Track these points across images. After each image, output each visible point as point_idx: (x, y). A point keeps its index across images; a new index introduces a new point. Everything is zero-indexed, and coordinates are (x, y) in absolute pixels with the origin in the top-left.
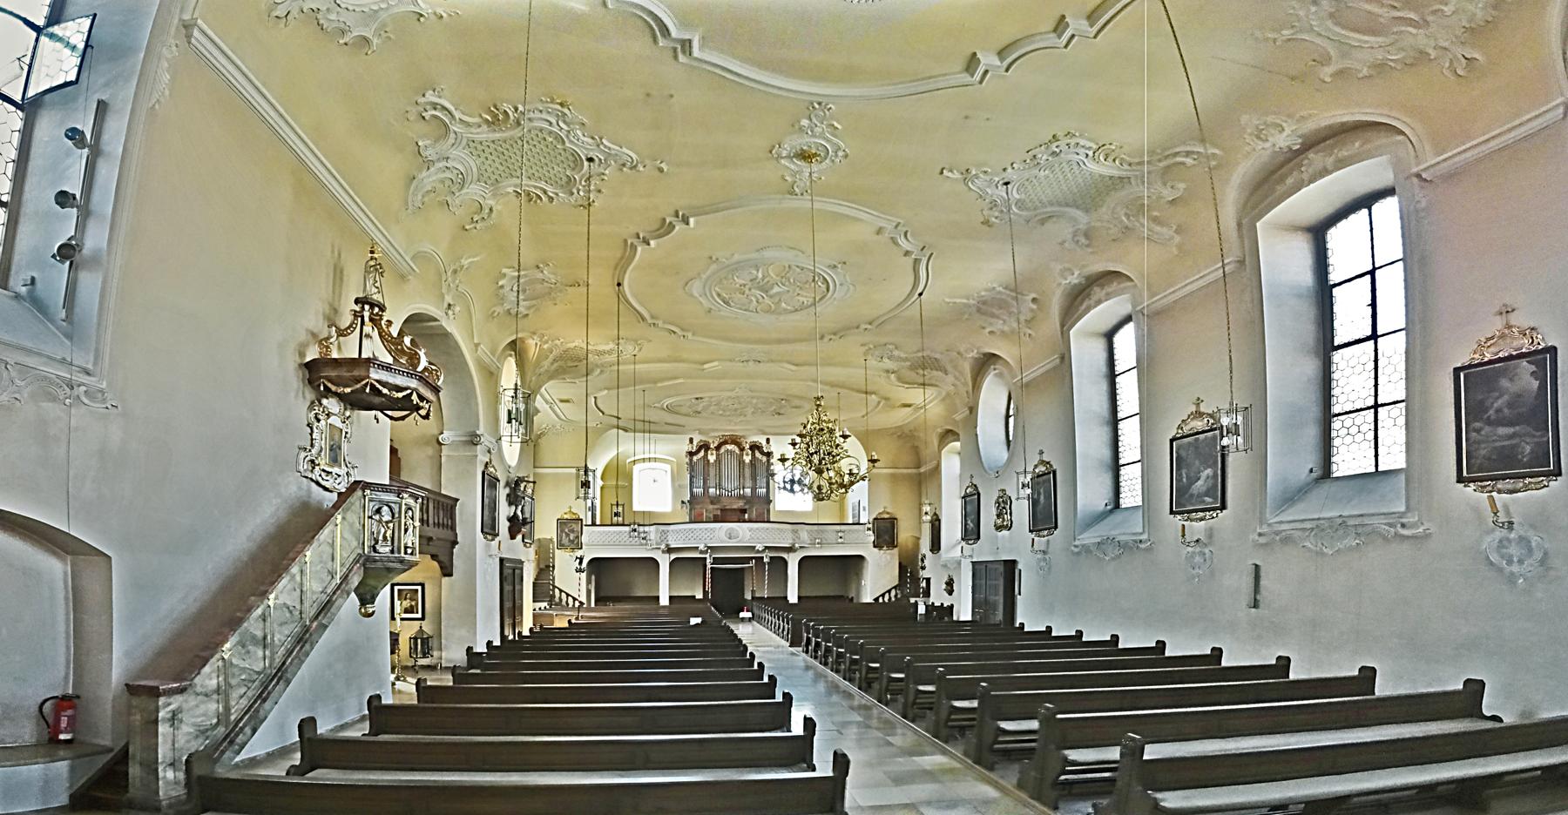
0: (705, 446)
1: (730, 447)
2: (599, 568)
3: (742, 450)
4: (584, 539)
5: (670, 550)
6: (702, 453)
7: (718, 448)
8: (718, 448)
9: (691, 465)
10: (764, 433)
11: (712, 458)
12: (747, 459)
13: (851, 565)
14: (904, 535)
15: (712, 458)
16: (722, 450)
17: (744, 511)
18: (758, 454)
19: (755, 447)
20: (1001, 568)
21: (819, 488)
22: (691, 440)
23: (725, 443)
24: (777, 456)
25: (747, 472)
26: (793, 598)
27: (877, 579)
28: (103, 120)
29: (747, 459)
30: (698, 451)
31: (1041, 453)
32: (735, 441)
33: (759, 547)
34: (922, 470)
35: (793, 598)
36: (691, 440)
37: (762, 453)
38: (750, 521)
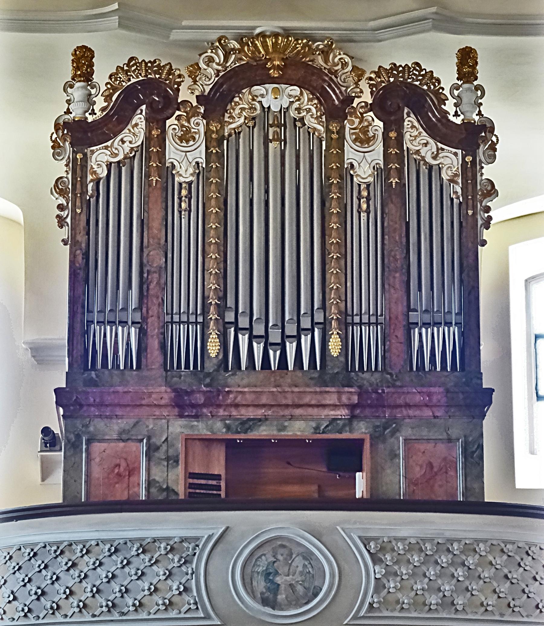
0: (148, 94)
1: (274, 98)
3: (337, 111)
7: (214, 105)
8: (214, 105)
9: (79, 196)
10: (449, 22)
11: (185, 159)
12: (365, 162)
15: (185, 159)
16: (237, 118)
17: (344, 456)
18: (416, 138)
19: (404, 96)
21: (197, 163)
22: (83, 60)
23: (251, 74)
24: (147, 429)
25: (363, 227)
28: (528, 289)
29: (365, 162)
32: (301, 67)
36: (83, 60)
37: (441, 131)
38: (375, 503)
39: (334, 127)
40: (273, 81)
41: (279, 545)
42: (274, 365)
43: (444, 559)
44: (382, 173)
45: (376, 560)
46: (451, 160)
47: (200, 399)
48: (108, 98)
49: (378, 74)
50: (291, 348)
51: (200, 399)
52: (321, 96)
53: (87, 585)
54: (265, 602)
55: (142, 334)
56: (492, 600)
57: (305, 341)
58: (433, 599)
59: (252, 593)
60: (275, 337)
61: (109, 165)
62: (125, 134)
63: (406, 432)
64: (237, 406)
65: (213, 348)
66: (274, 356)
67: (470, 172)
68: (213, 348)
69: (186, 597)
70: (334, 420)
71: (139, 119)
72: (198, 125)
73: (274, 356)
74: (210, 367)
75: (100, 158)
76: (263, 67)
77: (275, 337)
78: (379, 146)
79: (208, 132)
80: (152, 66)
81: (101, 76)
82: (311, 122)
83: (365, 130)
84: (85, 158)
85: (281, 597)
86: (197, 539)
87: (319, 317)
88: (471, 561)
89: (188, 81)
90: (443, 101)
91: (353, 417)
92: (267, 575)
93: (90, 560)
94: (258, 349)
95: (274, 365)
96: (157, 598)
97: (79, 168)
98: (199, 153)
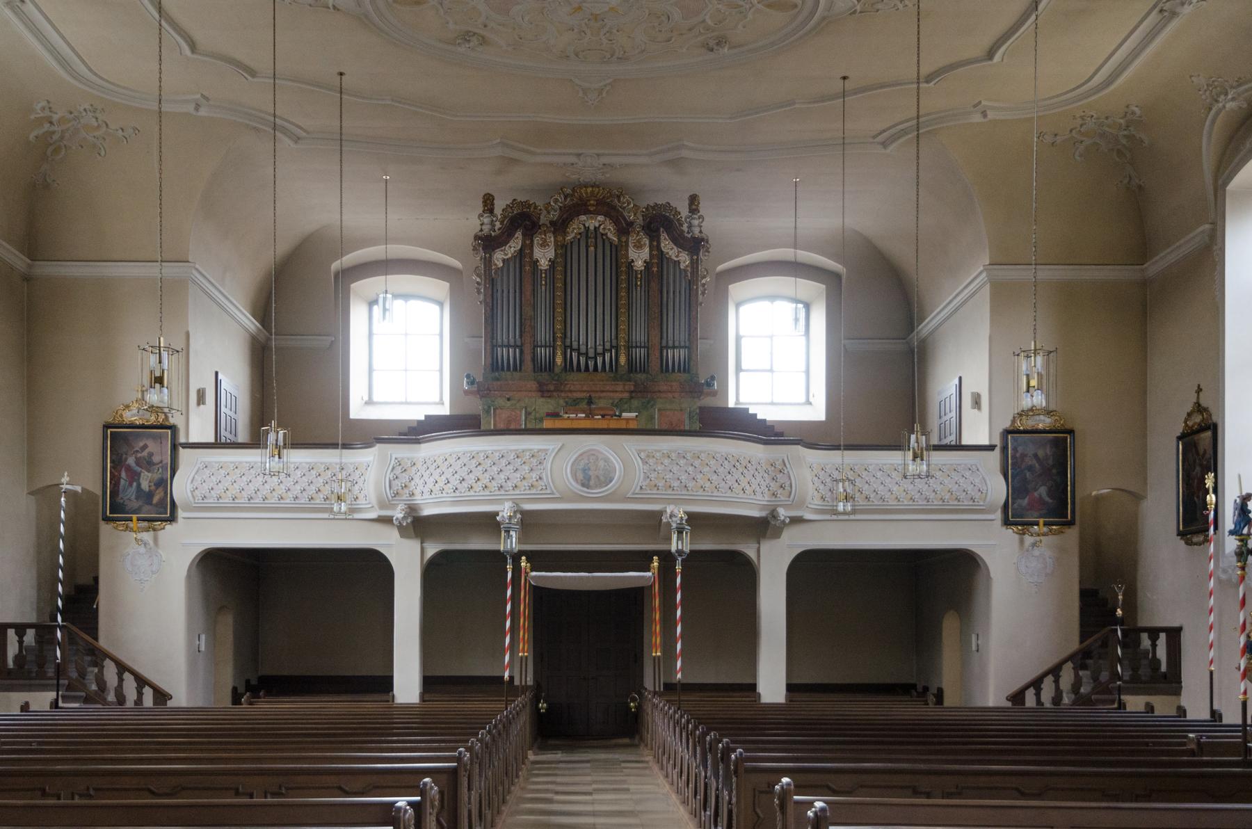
2: (242, 581)
3: (624, 229)
4: (181, 487)
5: (419, 526)
6: (514, 245)
8: (559, 226)
11: (544, 255)
12: (639, 257)
13: (932, 584)
14: (1094, 482)
15: (544, 255)
18: (667, 246)
20: (748, 681)
26: (772, 685)
27: (1013, 634)
30: (507, 234)
31: (1199, 390)
33: (676, 512)
34: (1154, 267)
35: (772, 685)
37: (680, 241)
39: (624, 239)
40: (591, 212)
41: (591, 454)
42: (591, 368)
43: (682, 462)
44: (648, 265)
45: (645, 463)
46: (684, 259)
47: (552, 388)
48: (502, 223)
49: (647, 209)
50: (599, 360)
51: (552, 388)
52: (616, 222)
53: (487, 475)
54: (583, 485)
55: (521, 352)
56: (708, 484)
57: (607, 356)
58: (676, 484)
59: (576, 480)
60: (591, 354)
61: (504, 261)
62: (512, 243)
63: (658, 406)
64: (571, 391)
65: (559, 360)
66: (591, 364)
67: (695, 264)
68: (559, 360)
69: (540, 482)
70: (621, 399)
71: (519, 234)
72: (551, 239)
73: (591, 364)
74: (557, 370)
75: (499, 257)
76: (585, 205)
77: (591, 354)
78: (647, 250)
79: (556, 241)
80: (525, 204)
81: (498, 211)
82: (610, 235)
83: (639, 241)
84: (491, 257)
85: (592, 483)
86: (546, 450)
87: (614, 343)
88: (697, 463)
89: (544, 212)
90: (681, 225)
91: (632, 398)
92: (584, 470)
93: (489, 462)
94: (582, 360)
95: (591, 368)
96: (525, 483)
97: (488, 262)
98: (550, 253)
